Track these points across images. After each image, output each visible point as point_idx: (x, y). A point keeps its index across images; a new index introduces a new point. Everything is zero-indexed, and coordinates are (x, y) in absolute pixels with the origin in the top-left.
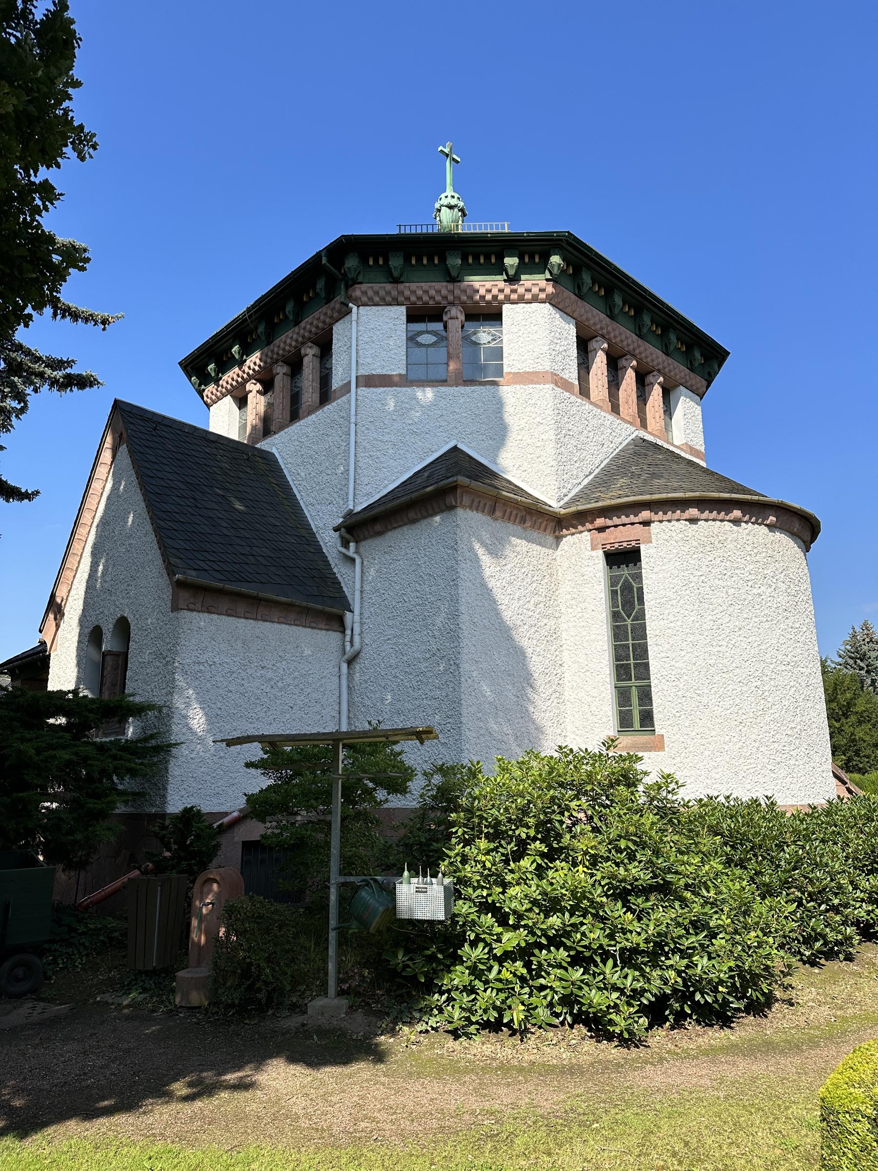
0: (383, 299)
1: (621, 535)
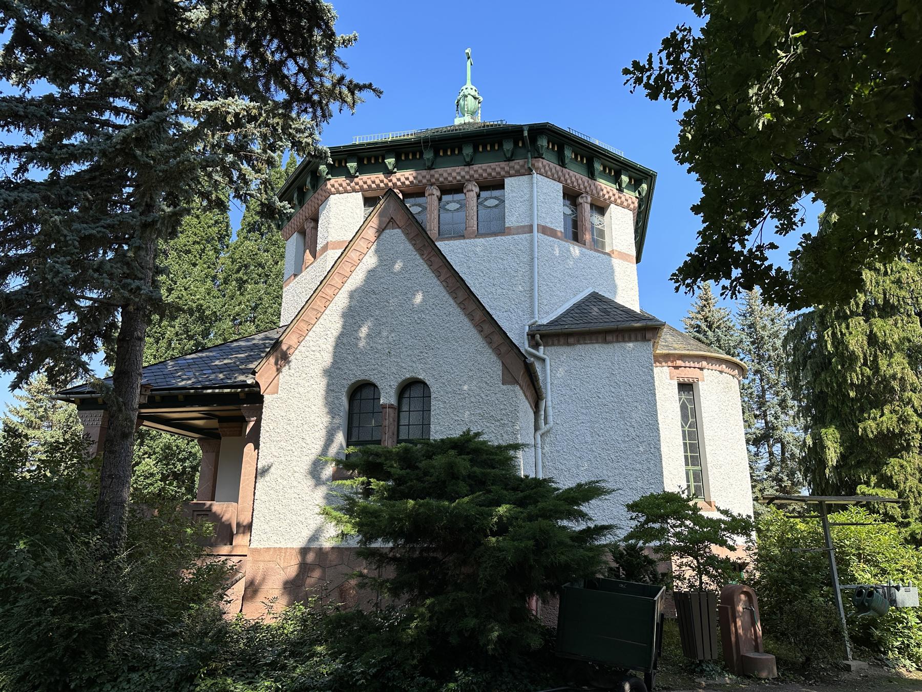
0: (553, 175)
1: (688, 373)
